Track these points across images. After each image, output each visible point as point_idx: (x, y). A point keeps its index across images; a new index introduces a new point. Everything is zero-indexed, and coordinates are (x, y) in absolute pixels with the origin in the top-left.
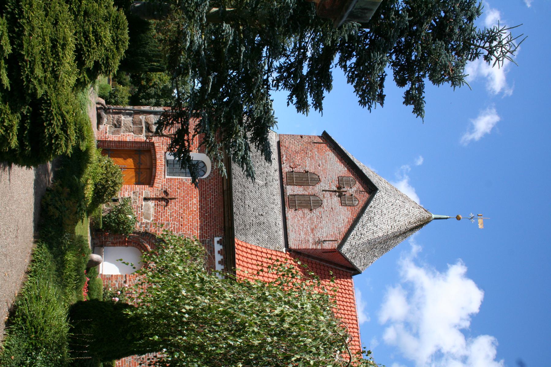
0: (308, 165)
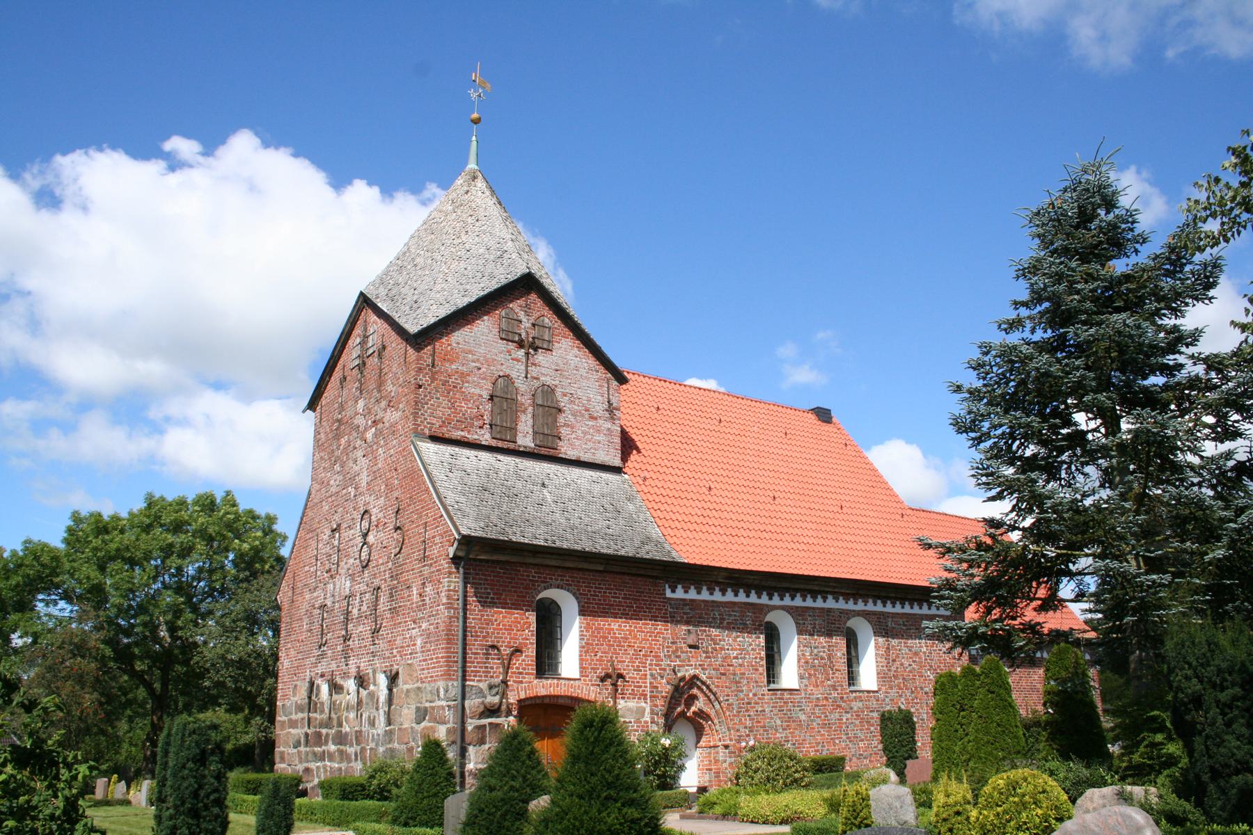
0: (477, 391)
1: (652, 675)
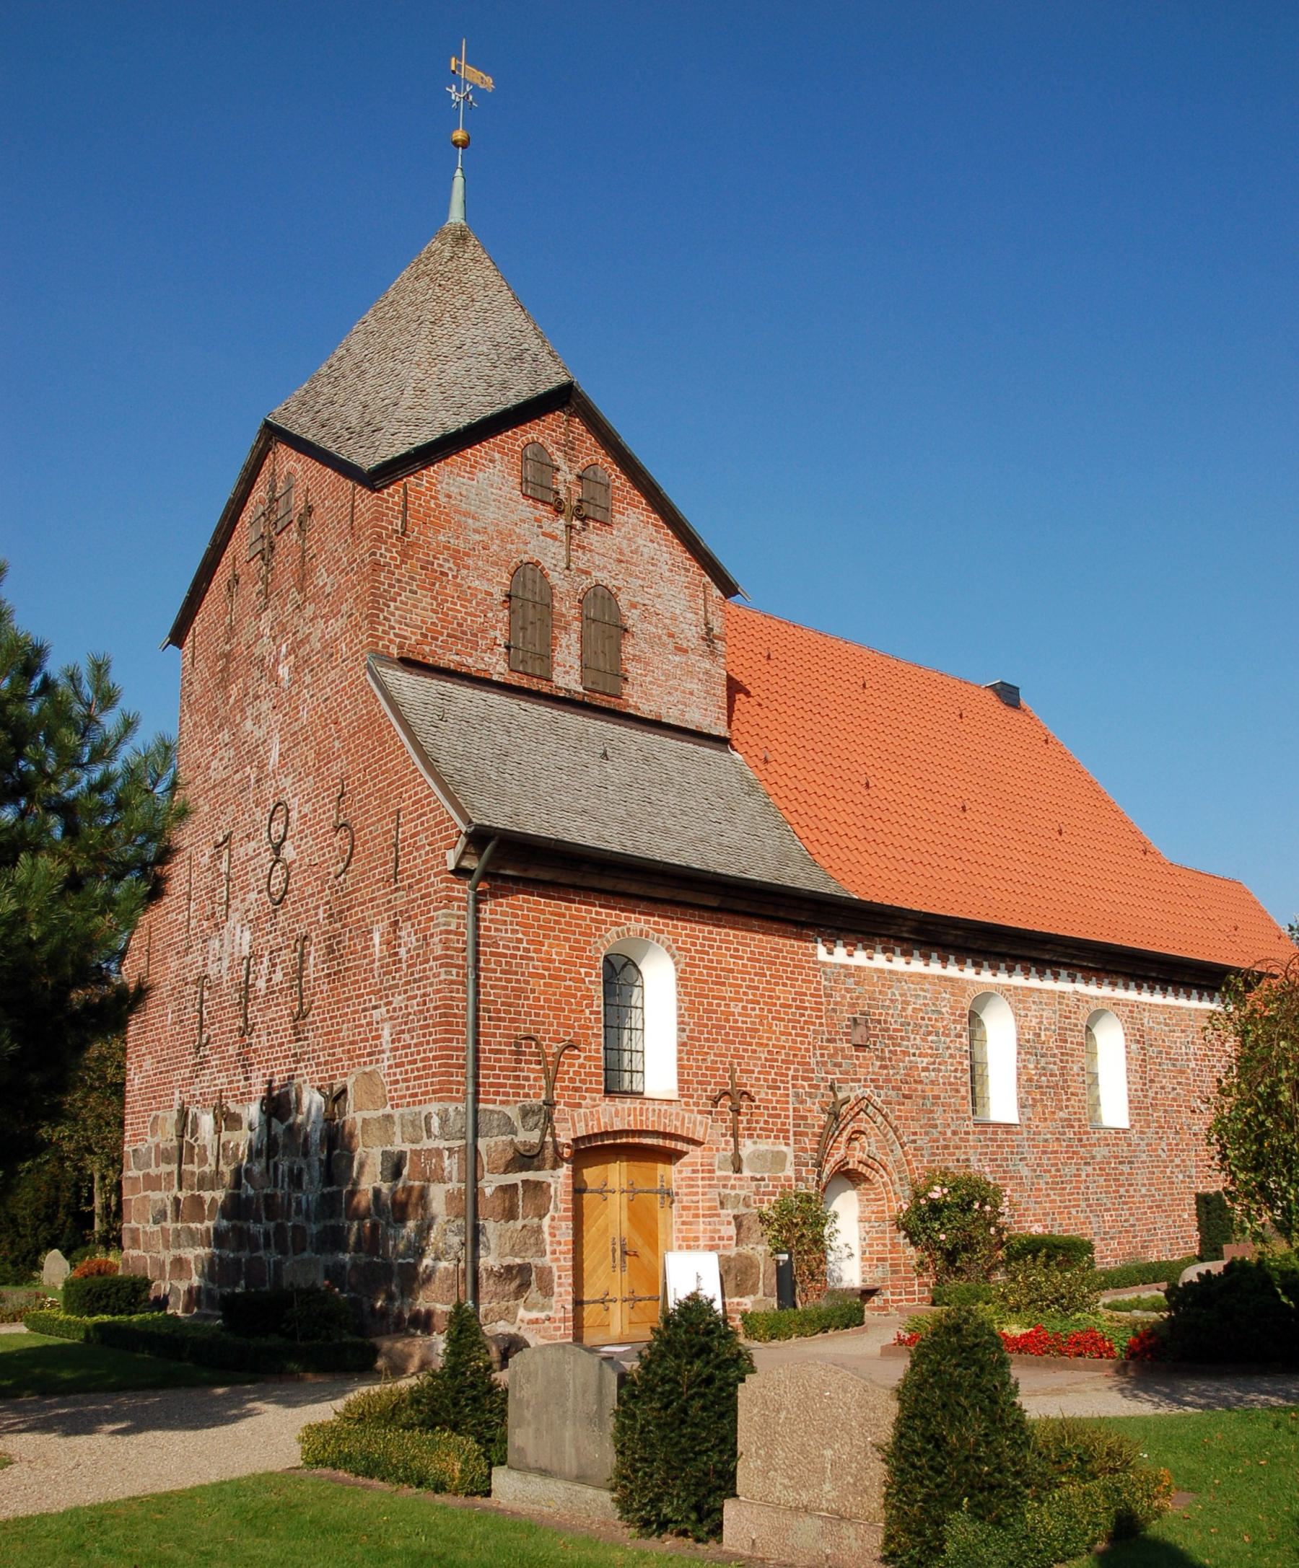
0: (485, 586)
1: (797, 1095)
